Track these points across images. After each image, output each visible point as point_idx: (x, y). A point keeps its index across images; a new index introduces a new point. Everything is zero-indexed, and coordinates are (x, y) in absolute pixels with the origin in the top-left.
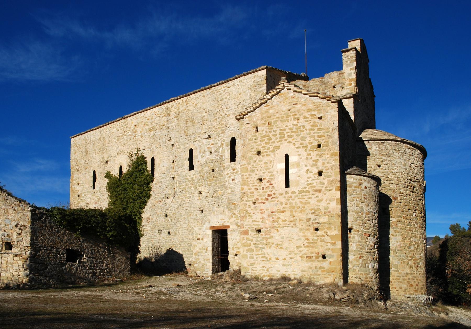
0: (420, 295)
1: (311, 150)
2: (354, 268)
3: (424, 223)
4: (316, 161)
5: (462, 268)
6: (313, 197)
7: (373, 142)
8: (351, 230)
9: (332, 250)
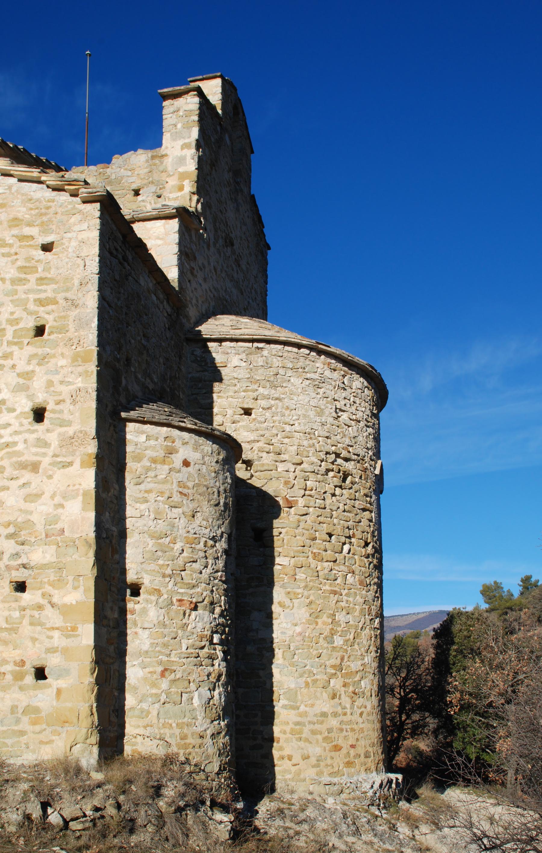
0: (363, 775)
1: (16, 344)
2: (145, 706)
3: (376, 574)
4: (28, 375)
5: (485, 689)
6: (14, 484)
7: (233, 344)
8: (136, 591)
9: (65, 651)
